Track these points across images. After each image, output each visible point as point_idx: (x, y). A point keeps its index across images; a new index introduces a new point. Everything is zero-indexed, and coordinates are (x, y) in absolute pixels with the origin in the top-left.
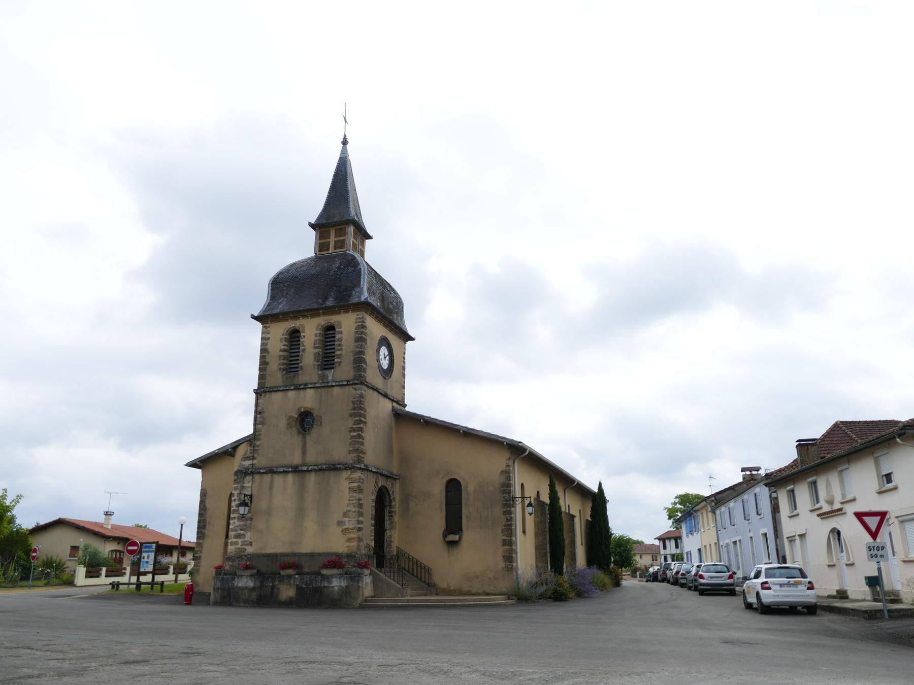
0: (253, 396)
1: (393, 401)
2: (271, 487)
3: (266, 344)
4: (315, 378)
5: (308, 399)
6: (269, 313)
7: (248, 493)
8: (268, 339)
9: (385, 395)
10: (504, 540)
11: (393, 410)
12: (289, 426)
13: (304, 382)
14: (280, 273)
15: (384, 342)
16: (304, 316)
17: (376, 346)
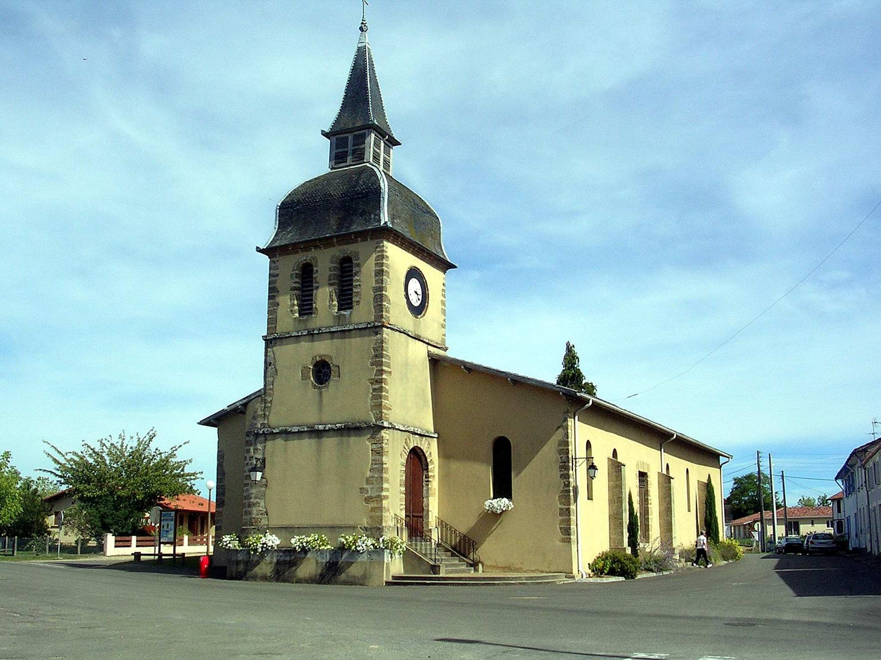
0: (263, 343)
1: (428, 344)
2: (286, 450)
3: (275, 282)
4: (329, 322)
5: (323, 348)
6: (277, 244)
7: (260, 456)
8: (277, 275)
9: (417, 338)
10: (561, 509)
11: (429, 354)
12: (305, 377)
13: (318, 326)
14: (295, 192)
15: (413, 273)
16: (316, 247)
17: (403, 280)
